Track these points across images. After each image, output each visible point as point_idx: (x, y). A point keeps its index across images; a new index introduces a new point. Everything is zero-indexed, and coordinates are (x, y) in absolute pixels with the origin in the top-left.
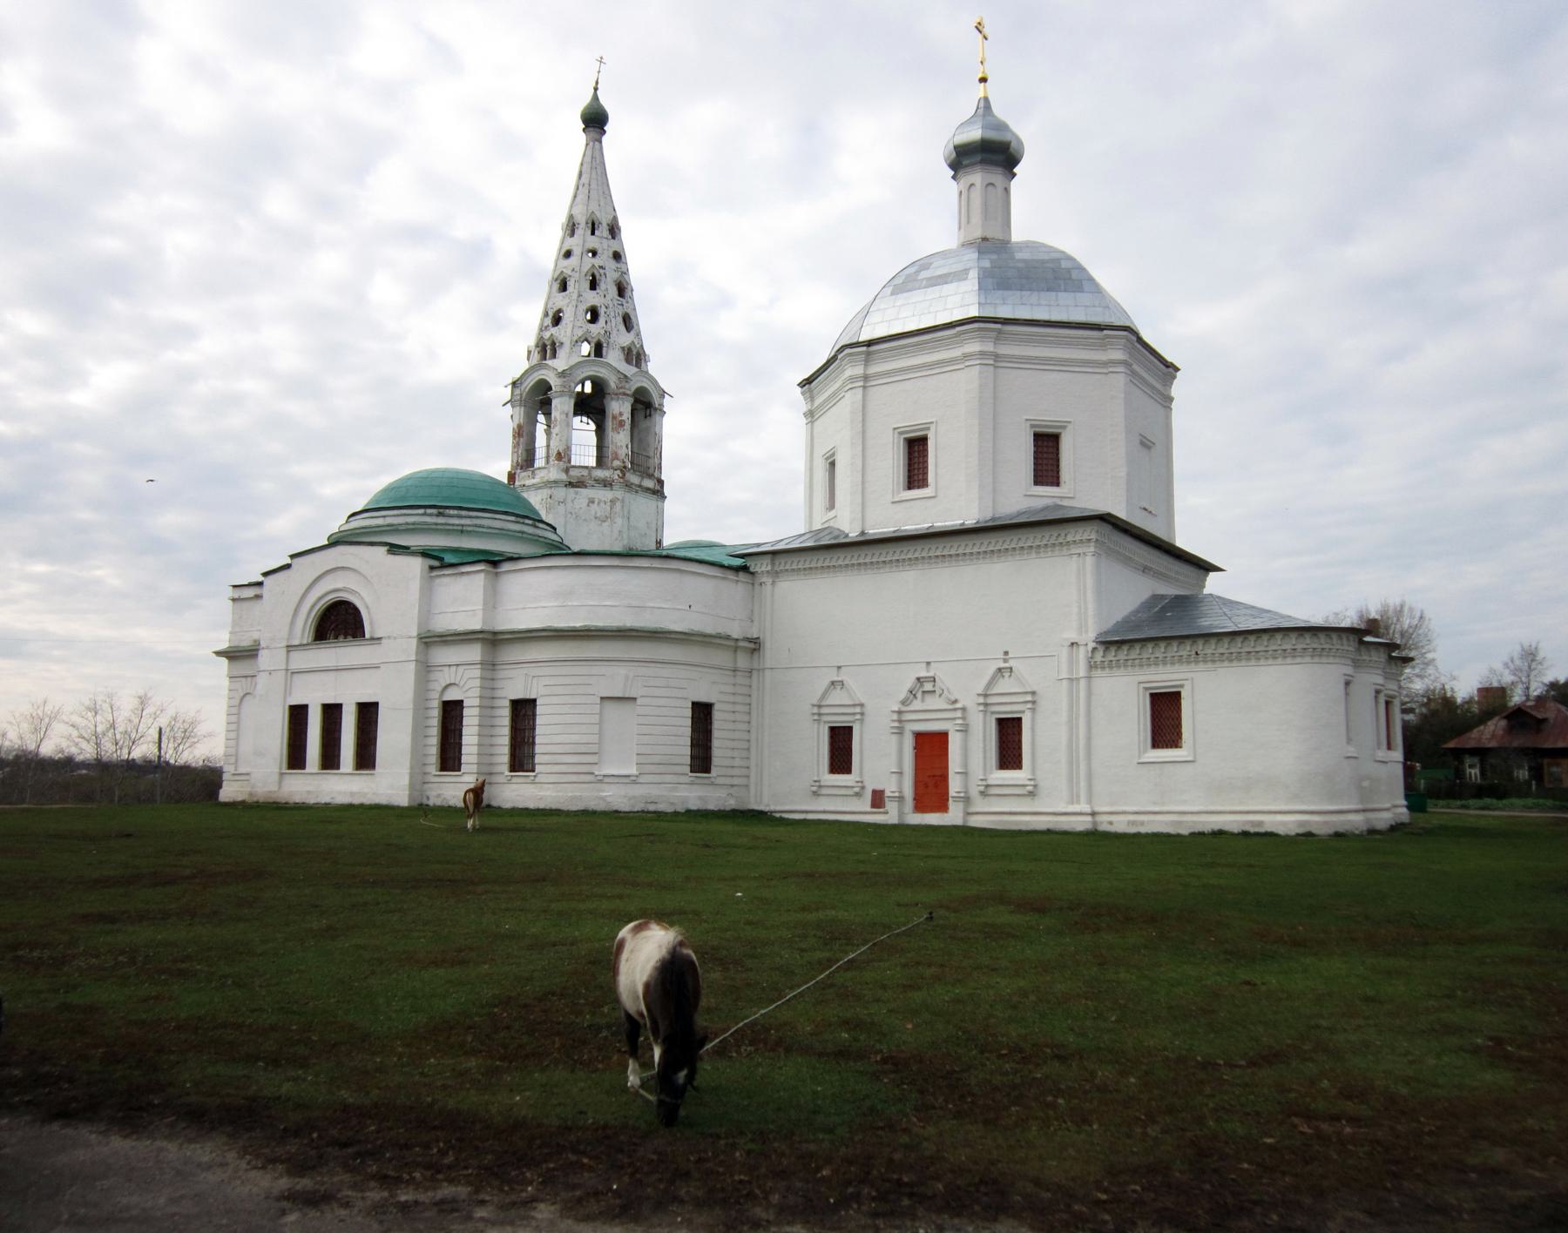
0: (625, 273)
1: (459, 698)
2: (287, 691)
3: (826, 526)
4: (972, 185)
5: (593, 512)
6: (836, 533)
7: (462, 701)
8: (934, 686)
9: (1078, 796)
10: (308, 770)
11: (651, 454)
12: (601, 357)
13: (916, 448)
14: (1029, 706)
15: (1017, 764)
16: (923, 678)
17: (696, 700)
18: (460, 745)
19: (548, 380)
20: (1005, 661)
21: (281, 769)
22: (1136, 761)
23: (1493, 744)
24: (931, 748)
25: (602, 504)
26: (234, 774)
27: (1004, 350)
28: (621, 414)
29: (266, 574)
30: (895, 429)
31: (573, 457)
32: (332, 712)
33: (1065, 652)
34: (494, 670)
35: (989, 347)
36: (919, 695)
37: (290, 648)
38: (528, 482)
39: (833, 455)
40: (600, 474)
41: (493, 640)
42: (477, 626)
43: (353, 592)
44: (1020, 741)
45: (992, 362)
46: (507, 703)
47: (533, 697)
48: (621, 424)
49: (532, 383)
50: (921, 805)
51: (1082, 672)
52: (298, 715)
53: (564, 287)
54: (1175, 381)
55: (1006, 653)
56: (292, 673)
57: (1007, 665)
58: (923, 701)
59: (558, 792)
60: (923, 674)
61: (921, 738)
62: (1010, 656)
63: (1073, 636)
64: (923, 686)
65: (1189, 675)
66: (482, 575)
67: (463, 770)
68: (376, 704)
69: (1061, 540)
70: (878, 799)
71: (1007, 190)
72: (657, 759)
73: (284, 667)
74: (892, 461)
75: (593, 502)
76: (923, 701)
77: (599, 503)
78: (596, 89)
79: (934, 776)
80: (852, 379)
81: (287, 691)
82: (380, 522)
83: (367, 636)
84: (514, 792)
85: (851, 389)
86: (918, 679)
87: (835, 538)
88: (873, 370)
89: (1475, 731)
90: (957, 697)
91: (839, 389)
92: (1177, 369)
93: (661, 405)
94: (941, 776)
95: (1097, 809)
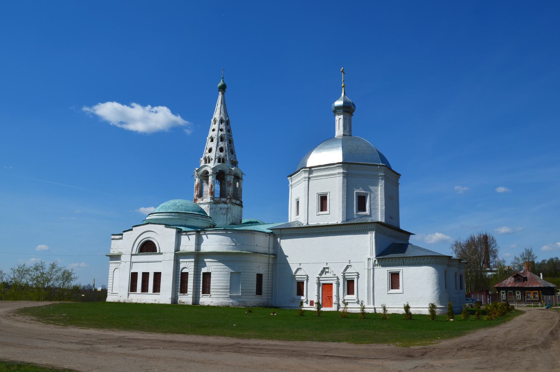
0: (231, 136)
1: (187, 272)
2: (131, 267)
3: (296, 220)
4: (340, 119)
5: (221, 212)
6: (299, 223)
7: (188, 272)
8: (329, 270)
9: (370, 303)
10: (137, 293)
11: (239, 193)
12: (224, 163)
13: (323, 199)
15: (397, 287)
17: (258, 273)
18: (187, 286)
19: (208, 170)
20: (350, 263)
21: (128, 292)
22: (387, 293)
23: (509, 286)
24: (326, 288)
25: (224, 210)
26: (111, 293)
28: (230, 181)
29: (132, 230)
30: (317, 193)
31: (215, 194)
32: (146, 275)
33: (366, 261)
34: (198, 263)
37: (132, 255)
38: (201, 202)
39: (298, 199)
40: (223, 199)
43: (153, 238)
44: (354, 287)
47: (210, 272)
48: (230, 184)
49: (202, 171)
51: (372, 267)
52: (134, 276)
53: (428, 364)
54: (400, 178)
55: (350, 261)
56: (132, 263)
57: (350, 264)
58: (325, 274)
59: (218, 300)
60: (325, 266)
62: (351, 262)
63: (369, 256)
65: (401, 269)
66: (195, 236)
67: (188, 293)
69: (366, 228)
71: (350, 120)
72: (219, 287)
74: (315, 203)
75: (221, 209)
76: (325, 274)
77: (223, 209)
79: (328, 297)
80: (305, 178)
81: (131, 267)
82: (161, 217)
83: (158, 252)
84: (205, 300)
85: (304, 181)
86: (324, 268)
87: (300, 225)
88: (311, 176)
89: (504, 281)
90: (335, 273)
91: (301, 180)
92: (400, 175)
93: (242, 177)
94: (330, 297)
95: (375, 307)
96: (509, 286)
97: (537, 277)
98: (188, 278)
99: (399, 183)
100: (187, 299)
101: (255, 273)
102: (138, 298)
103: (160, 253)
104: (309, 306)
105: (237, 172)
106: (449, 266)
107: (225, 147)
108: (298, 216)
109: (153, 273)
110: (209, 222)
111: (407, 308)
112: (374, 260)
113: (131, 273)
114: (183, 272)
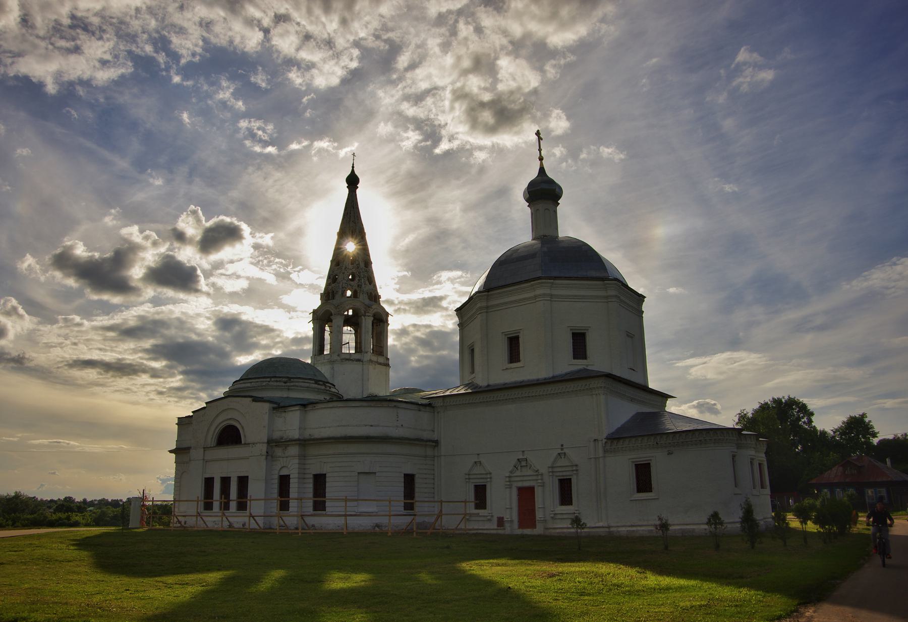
14: (575, 472)
16: (521, 459)
17: (405, 473)
23: (836, 481)
24: (526, 495)
27: (555, 292)
35: (548, 291)
36: (519, 468)
41: (304, 443)
42: (297, 436)
45: (549, 299)
46: (311, 476)
47: (324, 473)
50: (521, 525)
51: (601, 454)
52: (209, 483)
60: (521, 457)
61: (520, 489)
64: (522, 463)
67: (290, 511)
68: (213, 478)
70: (501, 522)
73: (202, 459)
74: (501, 349)
78: (353, 167)
83: (243, 442)
86: (518, 459)
96: (835, 481)
97: (879, 464)
98: (325, 484)
99: (643, 310)
100: (291, 520)
101: (311, 474)
102: (214, 520)
103: (247, 444)
104: (496, 527)
105: (379, 311)
106: (739, 447)
107: (357, 273)
108: (474, 375)
109: (236, 478)
110: (328, 392)
111: (664, 526)
112: (604, 442)
113: (204, 479)
114: (280, 474)
